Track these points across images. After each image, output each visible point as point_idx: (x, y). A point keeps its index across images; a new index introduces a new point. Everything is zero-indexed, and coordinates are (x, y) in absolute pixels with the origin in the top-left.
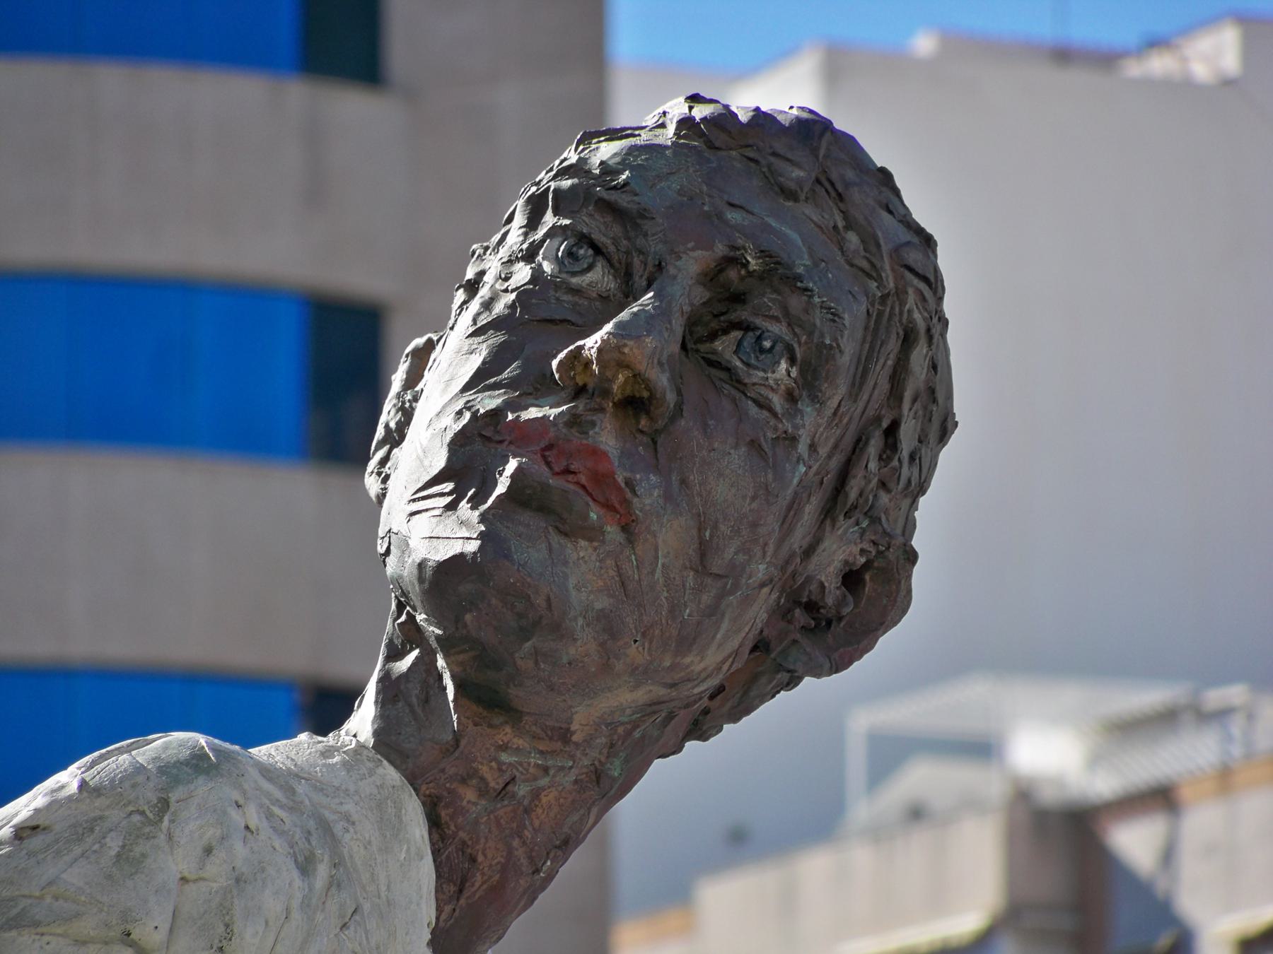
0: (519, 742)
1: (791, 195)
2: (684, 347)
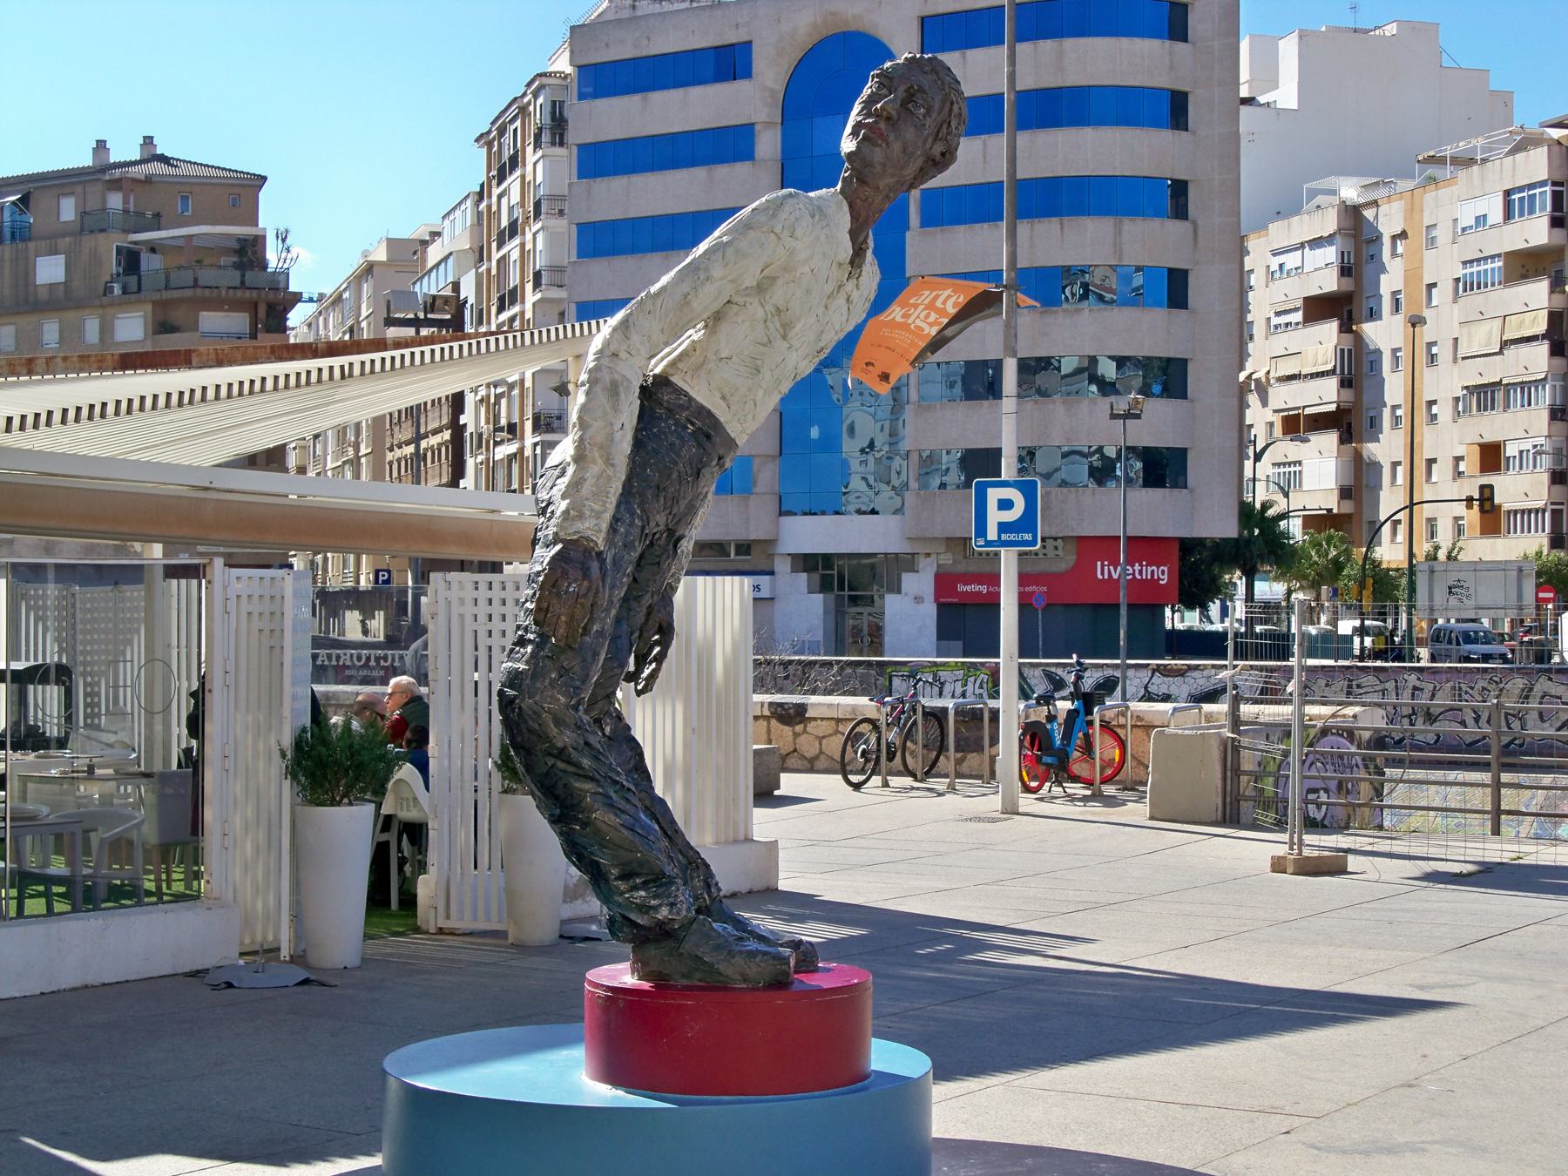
1: (926, 73)
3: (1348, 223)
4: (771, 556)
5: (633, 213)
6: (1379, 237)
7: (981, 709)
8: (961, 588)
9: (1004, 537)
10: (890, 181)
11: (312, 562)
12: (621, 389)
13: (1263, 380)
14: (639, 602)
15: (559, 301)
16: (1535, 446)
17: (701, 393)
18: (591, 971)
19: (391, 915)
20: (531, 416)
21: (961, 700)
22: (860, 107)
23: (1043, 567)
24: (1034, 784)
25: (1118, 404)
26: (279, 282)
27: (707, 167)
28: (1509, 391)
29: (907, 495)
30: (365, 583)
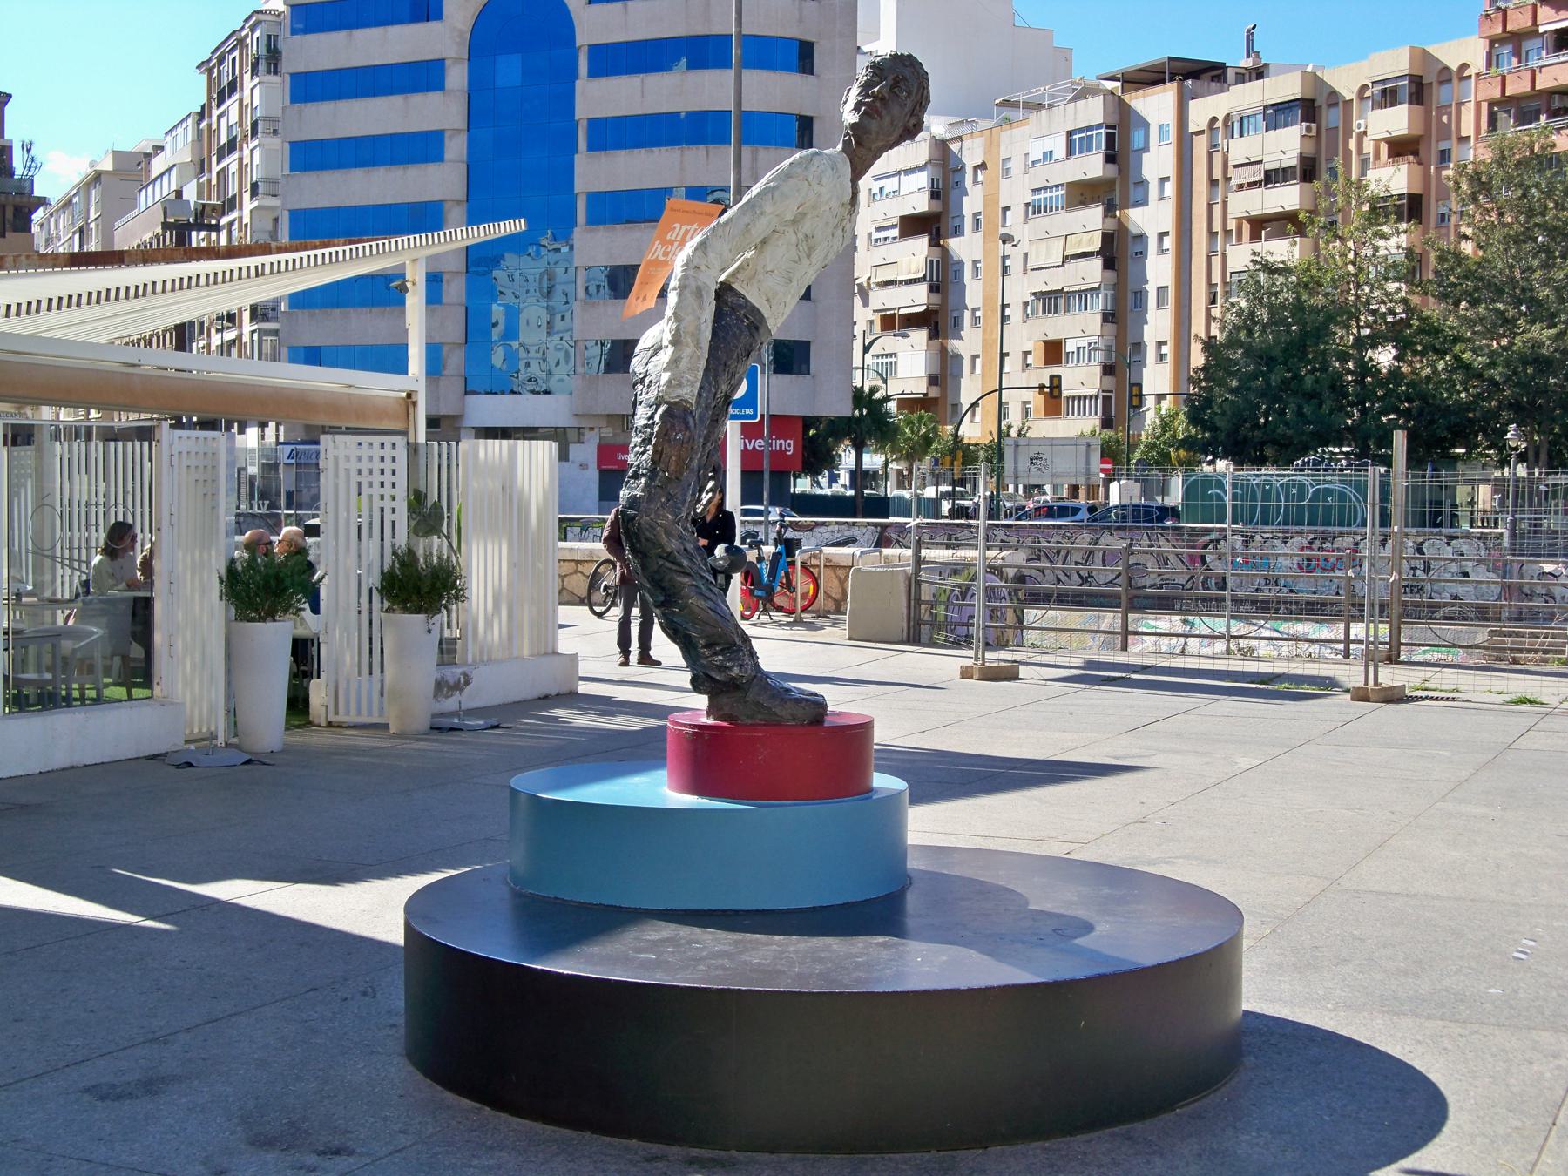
3: (937, 155)
6: (963, 167)
13: (865, 284)
16: (1090, 344)
17: (753, 296)
24: (747, 613)
26: (25, 188)
27: (404, 96)
28: (1069, 298)
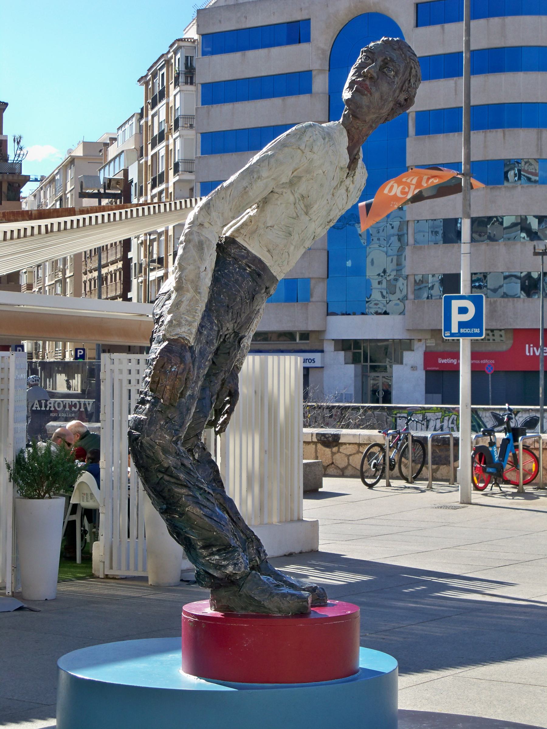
0: (360, 122)
1: (395, 50)
2: (379, 70)
4: (322, 341)
5: (236, 126)
7: (449, 438)
8: (440, 361)
9: (462, 331)
10: (373, 116)
11: (36, 344)
12: (205, 246)
14: (217, 377)
15: (189, 181)
18: (186, 605)
19: (77, 567)
20: (172, 253)
21: (439, 432)
22: (354, 71)
23: (491, 348)
24: (481, 485)
25: (538, 246)
26: (15, 169)
29: (407, 302)
30: (69, 358)
